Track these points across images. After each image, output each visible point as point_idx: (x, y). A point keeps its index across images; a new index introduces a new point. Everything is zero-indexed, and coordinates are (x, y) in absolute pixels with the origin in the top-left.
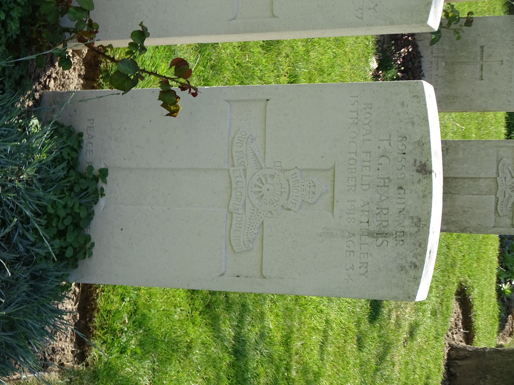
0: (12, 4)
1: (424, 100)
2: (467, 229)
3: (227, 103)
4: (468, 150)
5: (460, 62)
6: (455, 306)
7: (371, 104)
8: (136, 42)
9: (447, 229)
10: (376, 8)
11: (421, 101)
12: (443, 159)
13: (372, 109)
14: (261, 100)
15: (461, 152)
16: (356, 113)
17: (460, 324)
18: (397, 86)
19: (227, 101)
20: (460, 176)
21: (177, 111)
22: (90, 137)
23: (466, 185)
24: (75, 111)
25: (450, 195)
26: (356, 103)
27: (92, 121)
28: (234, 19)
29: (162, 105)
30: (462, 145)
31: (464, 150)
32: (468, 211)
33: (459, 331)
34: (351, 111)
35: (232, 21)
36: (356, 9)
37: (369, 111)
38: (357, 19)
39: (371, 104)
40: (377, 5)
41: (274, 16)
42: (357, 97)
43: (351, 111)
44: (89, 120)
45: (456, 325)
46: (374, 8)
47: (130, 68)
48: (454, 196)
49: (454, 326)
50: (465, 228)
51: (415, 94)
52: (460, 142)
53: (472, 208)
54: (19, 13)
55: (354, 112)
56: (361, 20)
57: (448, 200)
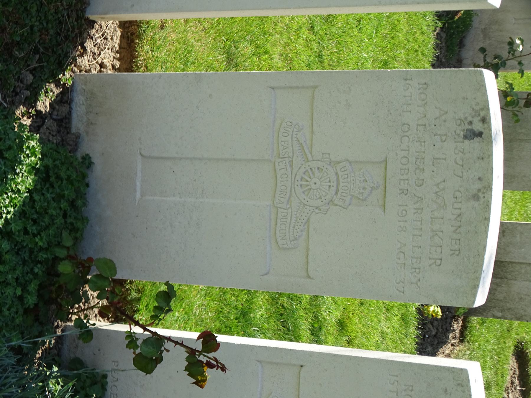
0: (29, 275)
1: (469, 390)
2: (524, 318)
3: (258, 363)
4: (525, 234)
5: (519, 139)
6: (512, 363)
7: (412, 386)
8: (161, 305)
9: (503, 316)
10: (419, 283)
11: (466, 390)
12: (498, 242)
13: (413, 392)
14: (294, 365)
15: (518, 236)
16: (395, 394)
17: (517, 382)
18: (440, 371)
19: (258, 361)
20: (517, 261)
21: (204, 381)
22: (115, 379)
23: (523, 271)
24: (99, 350)
25: (506, 280)
26: (396, 383)
27: (116, 364)
28: (267, 274)
29: (188, 375)
30: (519, 228)
31: (522, 233)
32: (525, 299)
33: (515, 389)
34: (391, 391)
35: (265, 277)
36: (398, 281)
37: (410, 394)
38: (398, 292)
39: (412, 386)
40: (419, 280)
41: (309, 277)
42: (397, 376)
43: (391, 391)
44: (113, 362)
45: (512, 383)
46: (416, 283)
47: (154, 348)
48: (510, 282)
49: (509, 385)
50: (522, 317)
51: (459, 382)
52: (517, 225)
53: (529, 296)
54: (36, 285)
55: (394, 392)
56: (402, 294)
57: (503, 285)
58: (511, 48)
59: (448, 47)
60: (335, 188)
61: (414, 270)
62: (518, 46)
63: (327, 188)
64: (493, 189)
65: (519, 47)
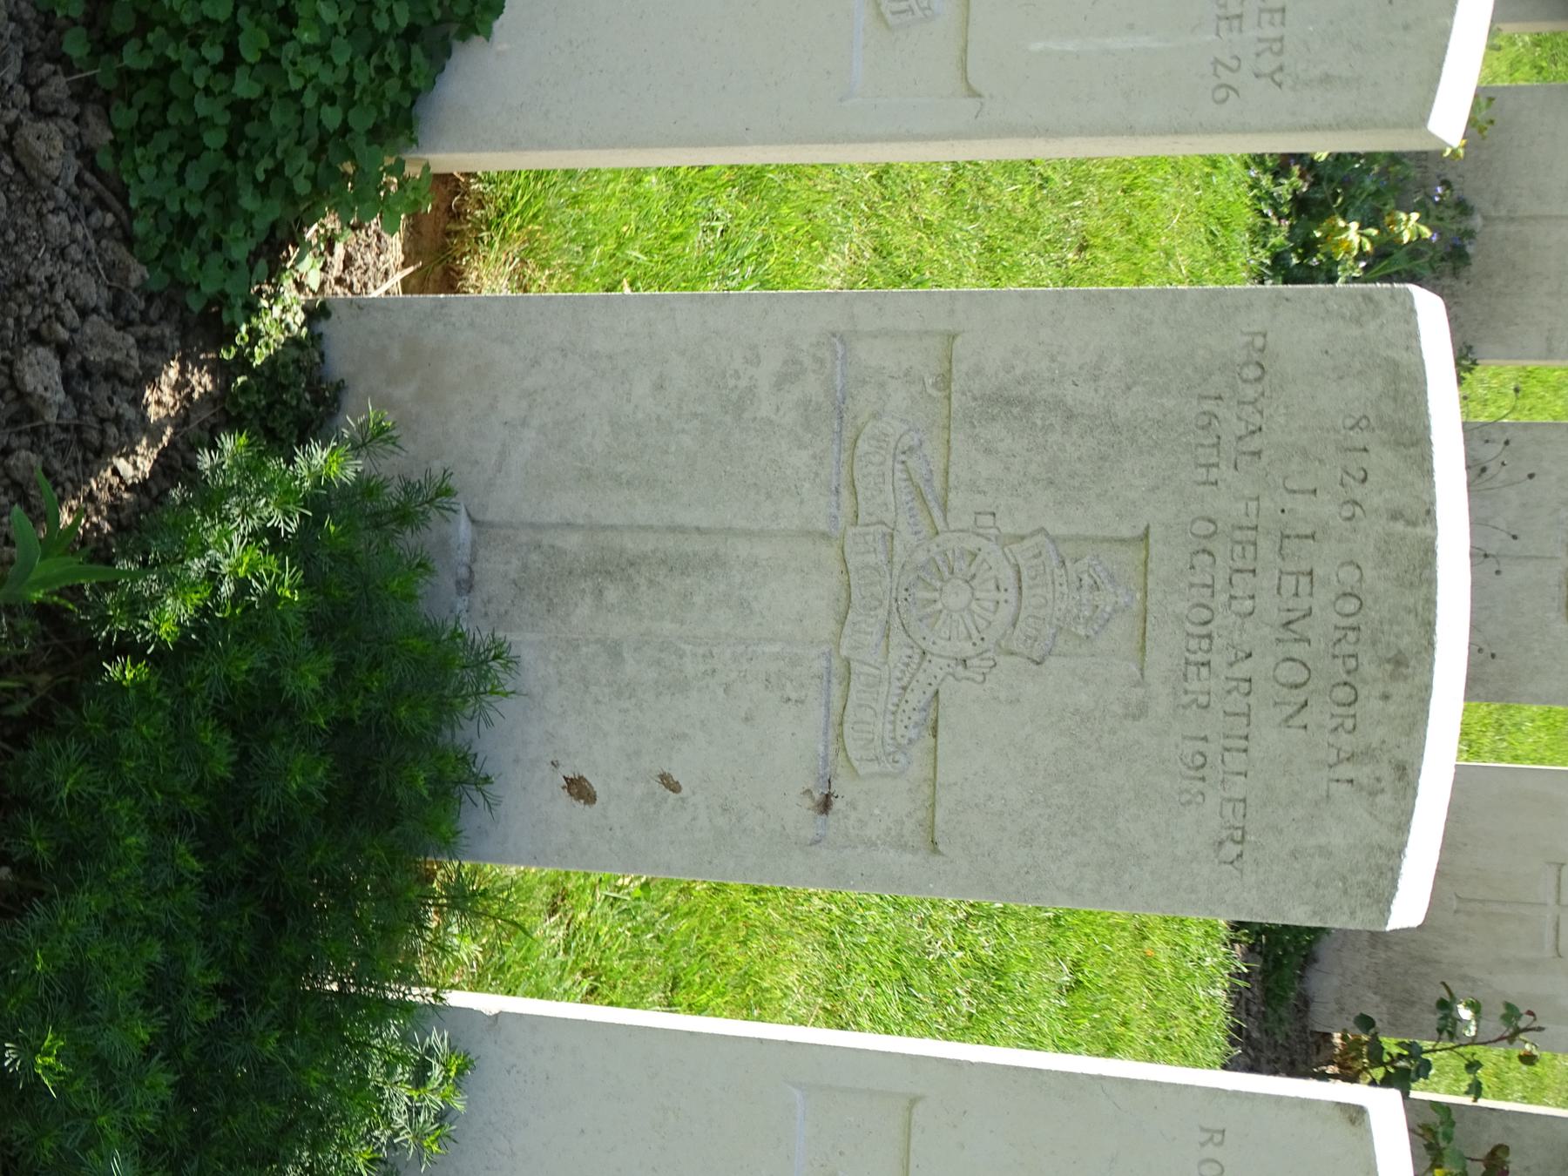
58: (1445, 1018)
59: (1267, 990)
60: (1012, 608)
61: (1207, 1136)
62: (1467, 1024)
63: (991, 606)
64: (1438, 646)
65: (1467, 1027)
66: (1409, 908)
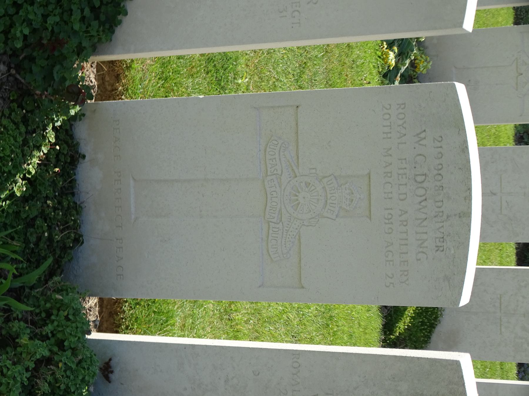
66: (468, 25)
